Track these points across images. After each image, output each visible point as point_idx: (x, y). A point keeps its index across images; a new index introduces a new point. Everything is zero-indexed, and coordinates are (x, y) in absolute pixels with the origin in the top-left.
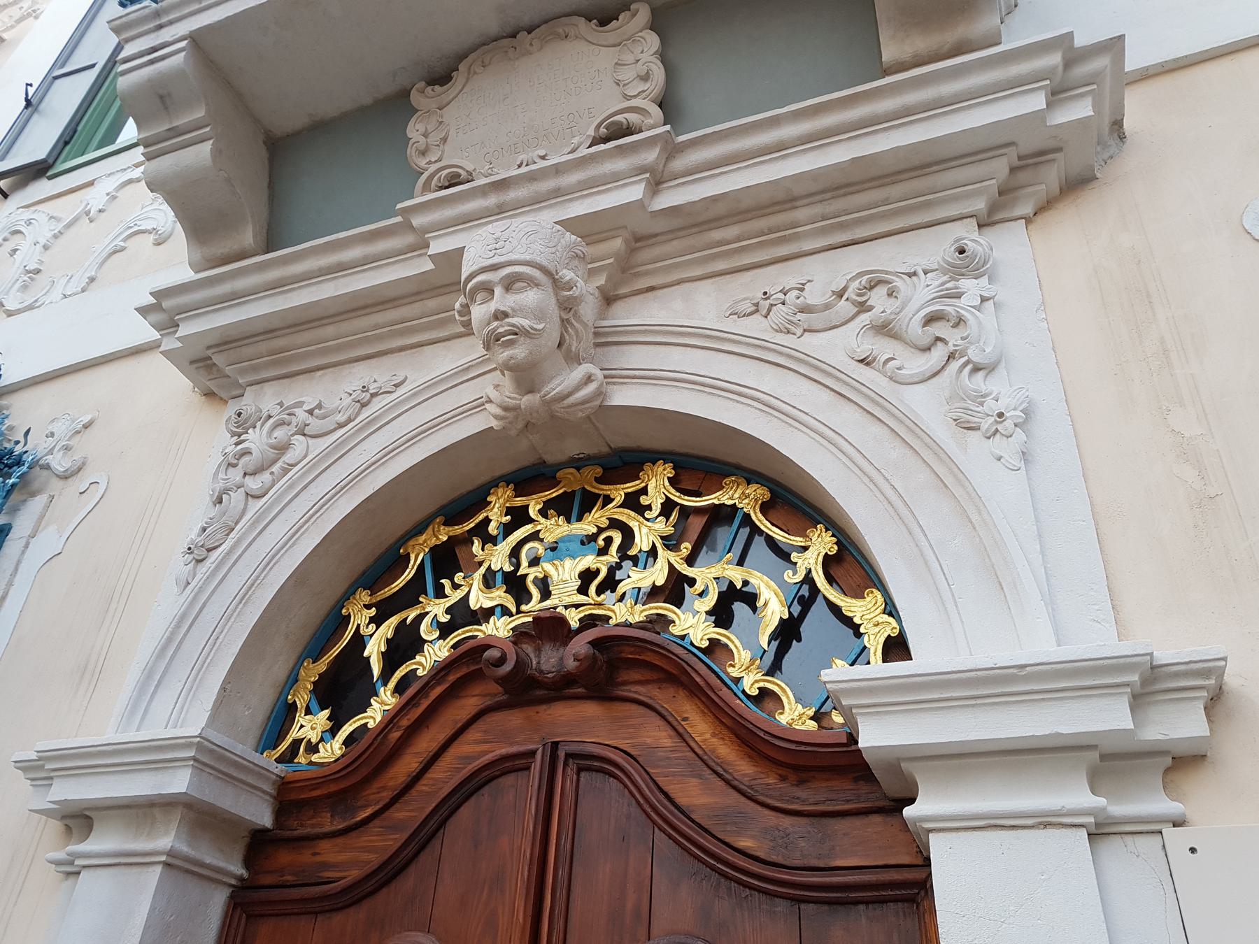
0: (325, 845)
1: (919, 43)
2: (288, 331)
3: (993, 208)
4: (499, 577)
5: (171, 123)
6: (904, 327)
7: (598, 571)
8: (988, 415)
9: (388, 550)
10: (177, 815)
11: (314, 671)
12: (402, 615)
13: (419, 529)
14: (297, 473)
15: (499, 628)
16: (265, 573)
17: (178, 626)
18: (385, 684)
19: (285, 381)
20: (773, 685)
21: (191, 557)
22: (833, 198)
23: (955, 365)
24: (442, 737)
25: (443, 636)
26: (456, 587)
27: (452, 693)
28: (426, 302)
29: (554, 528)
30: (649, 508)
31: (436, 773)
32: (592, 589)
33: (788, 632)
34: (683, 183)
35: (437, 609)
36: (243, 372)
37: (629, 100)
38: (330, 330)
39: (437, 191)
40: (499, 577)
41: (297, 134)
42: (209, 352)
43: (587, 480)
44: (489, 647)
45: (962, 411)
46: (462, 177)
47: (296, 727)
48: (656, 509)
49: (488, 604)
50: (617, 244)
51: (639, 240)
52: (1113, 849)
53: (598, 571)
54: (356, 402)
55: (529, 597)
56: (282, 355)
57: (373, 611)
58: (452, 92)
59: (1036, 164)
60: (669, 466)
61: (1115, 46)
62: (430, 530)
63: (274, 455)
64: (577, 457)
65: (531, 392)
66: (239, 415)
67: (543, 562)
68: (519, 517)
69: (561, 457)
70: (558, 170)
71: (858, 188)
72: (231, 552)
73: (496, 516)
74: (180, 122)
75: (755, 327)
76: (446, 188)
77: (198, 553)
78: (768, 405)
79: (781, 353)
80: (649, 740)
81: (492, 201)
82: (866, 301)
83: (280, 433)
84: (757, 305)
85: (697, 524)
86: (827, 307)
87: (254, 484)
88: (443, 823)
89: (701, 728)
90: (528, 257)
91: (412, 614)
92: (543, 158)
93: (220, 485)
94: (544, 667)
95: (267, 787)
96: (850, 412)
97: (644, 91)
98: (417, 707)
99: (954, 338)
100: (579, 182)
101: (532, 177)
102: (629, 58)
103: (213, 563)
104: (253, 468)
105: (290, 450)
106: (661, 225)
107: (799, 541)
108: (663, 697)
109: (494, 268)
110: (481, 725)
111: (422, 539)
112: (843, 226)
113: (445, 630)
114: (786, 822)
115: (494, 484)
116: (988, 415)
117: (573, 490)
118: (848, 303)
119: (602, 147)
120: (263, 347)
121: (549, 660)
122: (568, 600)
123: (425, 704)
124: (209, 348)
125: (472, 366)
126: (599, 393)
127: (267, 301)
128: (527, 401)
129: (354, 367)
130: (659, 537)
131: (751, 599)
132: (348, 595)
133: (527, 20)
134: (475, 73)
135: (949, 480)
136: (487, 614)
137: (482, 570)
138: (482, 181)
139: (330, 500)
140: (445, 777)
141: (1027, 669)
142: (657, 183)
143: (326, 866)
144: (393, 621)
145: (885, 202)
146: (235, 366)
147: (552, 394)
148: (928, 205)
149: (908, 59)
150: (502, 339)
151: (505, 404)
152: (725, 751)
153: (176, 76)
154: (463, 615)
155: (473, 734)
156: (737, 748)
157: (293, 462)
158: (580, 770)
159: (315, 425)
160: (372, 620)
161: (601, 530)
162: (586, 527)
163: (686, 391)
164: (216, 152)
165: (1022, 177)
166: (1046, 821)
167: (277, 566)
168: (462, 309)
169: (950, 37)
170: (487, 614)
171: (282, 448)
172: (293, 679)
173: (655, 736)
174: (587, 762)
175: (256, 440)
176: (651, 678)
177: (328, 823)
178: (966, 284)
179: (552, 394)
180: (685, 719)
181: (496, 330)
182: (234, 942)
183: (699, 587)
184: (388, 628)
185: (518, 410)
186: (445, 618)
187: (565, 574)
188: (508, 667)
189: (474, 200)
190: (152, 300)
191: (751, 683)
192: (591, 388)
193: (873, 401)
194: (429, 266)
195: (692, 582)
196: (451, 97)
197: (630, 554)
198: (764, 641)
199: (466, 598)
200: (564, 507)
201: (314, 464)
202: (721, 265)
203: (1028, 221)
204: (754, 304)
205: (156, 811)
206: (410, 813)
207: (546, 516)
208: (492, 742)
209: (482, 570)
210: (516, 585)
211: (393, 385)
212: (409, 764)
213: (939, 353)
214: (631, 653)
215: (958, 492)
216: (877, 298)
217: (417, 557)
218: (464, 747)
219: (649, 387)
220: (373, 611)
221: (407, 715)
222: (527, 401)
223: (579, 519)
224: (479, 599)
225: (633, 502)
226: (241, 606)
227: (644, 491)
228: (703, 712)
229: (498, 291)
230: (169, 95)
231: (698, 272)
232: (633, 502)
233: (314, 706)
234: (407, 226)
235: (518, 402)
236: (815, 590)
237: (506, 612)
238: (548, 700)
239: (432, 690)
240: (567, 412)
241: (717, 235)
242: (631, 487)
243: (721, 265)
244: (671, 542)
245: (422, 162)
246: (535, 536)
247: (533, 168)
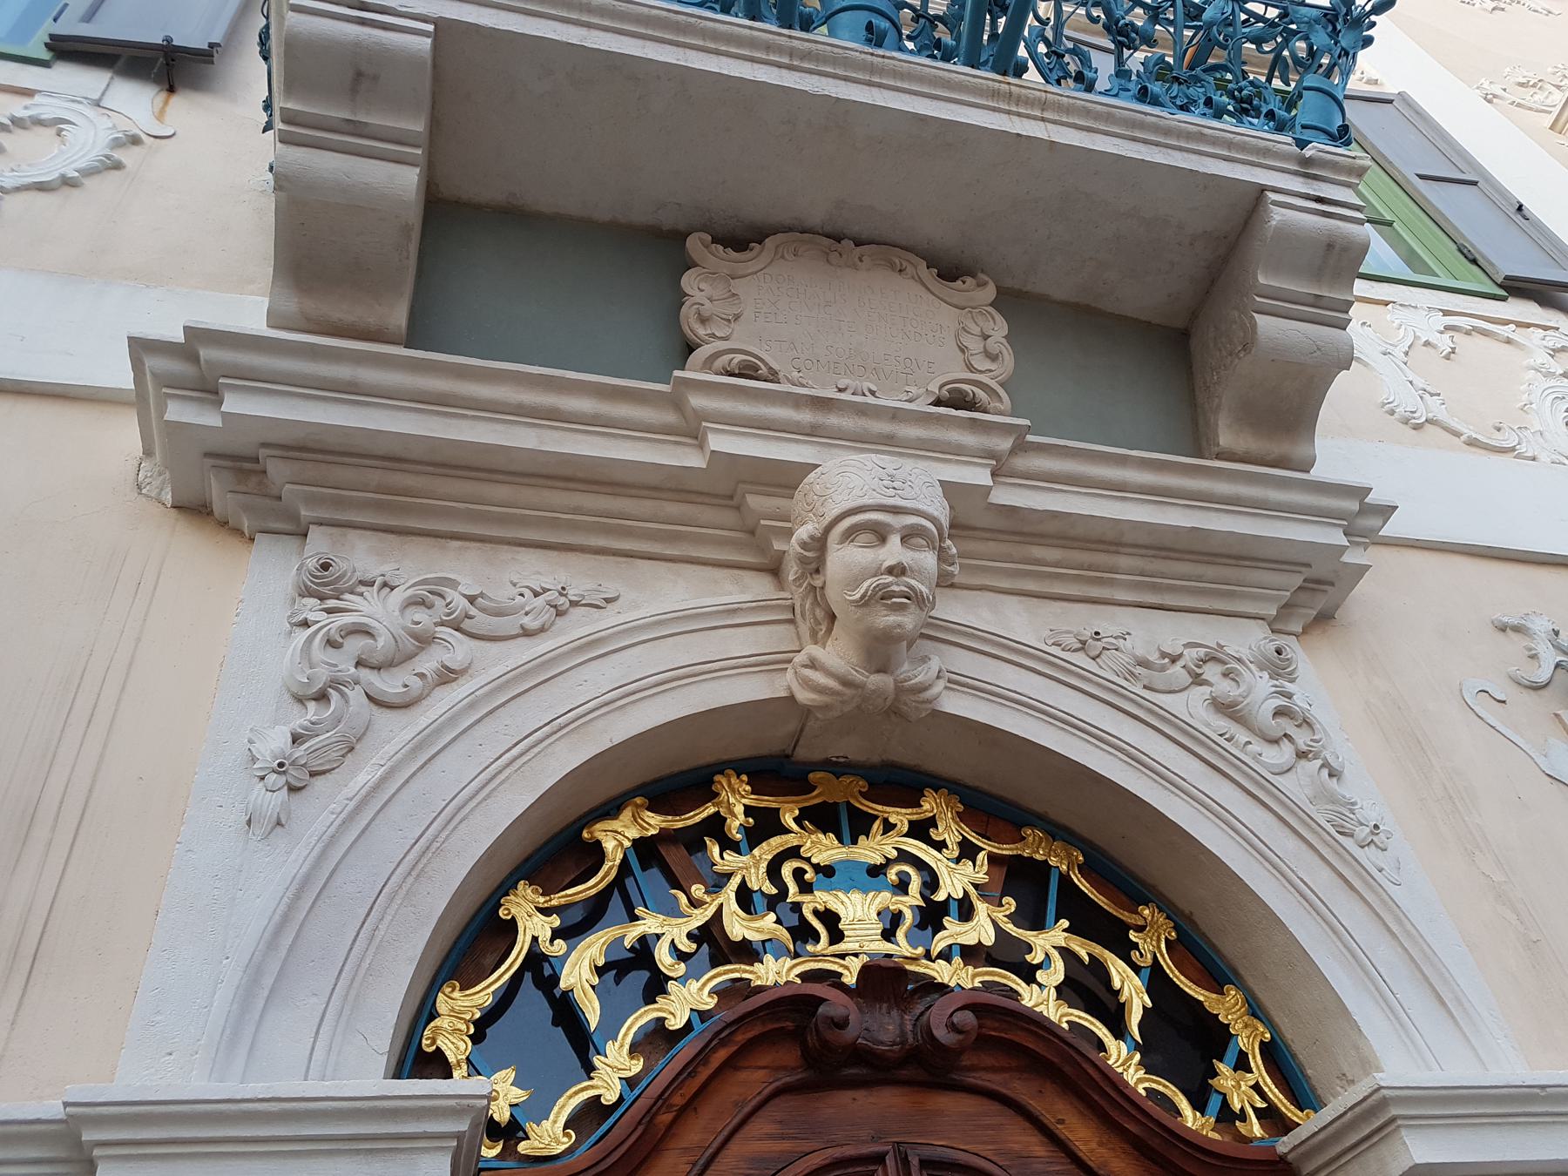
2: (430, 469)
5: (355, 115)
6: (1254, 712)
8: (1362, 824)
13: (610, 810)
14: (482, 687)
16: (446, 833)
17: (297, 897)
19: (391, 537)
21: (282, 779)
22: (1153, 556)
26: (695, 903)
28: (665, 504)
29: (824, 849)
34: (1020, 485)
36: (311, 500)
37: (972, 372)
38: (502, 492)
39: (722, 375)
42: (263, 452)
43: (850, 791)
45: (1338, 815)
46: (760, 372)
54: (552, 606)
56: (409, 499)
57: (556, 921)
58: (753, 266)
59: (1313, 589)
61: (1387, 511)
62: (627, 814)
63: (413, 648)
64: (834, 759)
65: (882, 670)
66: (325, 567)
67: (817, 890)
69: (817, 755)
70: (895, 415)
71: (1177, 555)
72: (378, 787)
74: (374, 119)
76: (732, 375)
79: (1140, 706)
80: (1016, 1147)
81: (806, 417)
82: (1201, 674)
84: (1084, 643)
92: (873, 393)
93: (323, 675)
97: (990, 371)
98: (693, 1077)
99: (1302, 738)
100: (919, 439)
101: (862, 410)
103: (351, 799)
104: (381, 658)
105: (434, 646)
109: (896, 510)
112: (1155, 588)
116: (1362, 824)
117: (835, 802)
118: (1183, 671)
120: (375, 477)
124: (265, 445)
125: (741, 609)
127: (413, 416)
128: (875, 681)
129: (518, 552)
132: (506, 887)
133: (855, 229)
134: (783, 257)
137: (734, 883)
139: (541, 741)
141: (1548, 1090)
145: (1199, 579)
146: (306, 488)
147: (913, 681)
148: (1231, 595)
149: (1240, 453)
150: (894, 600)
151: (850, 677)
156: (1135, 1162)
157: (457, 668)
159: (481, 622)
160: (556, 934)
163: (1031, 719)
167: (463, 825)
168: (811, 541)
169: (1276, 448)
171: (424, 641)
172: (425, 1012)
176: (1007, 1066)
179: (913, 681)
180: (1061, 1122)
181: (889, 586)
184: (594, 947)
185: (860, 690)
189: (781, 406)
190: (179, 337)
193: (1257, 783)
196: (750, 271)
197: (935, 899)
200: (822, 818)
201: (508, 682)
202: (1031, 586)
204: (1080, 641)
208: (796, 1138)
209: (734, 883)
211: (604, 599)
214: (995, 1029)
219: (983, 703)
220: (556, 921)
221: (681, 1089)
222: (875, 681)
226: (411, 880)
228: (1081, 1113)
229: (895, 540)
230: (375, 78)
231: (1005, 584)
234: (675, 403)
235: (865, 679)
239: (714, 1053)
240: (917, 708)
241: (1038, 552)
243: (1031, 586)
247: (869, 402)
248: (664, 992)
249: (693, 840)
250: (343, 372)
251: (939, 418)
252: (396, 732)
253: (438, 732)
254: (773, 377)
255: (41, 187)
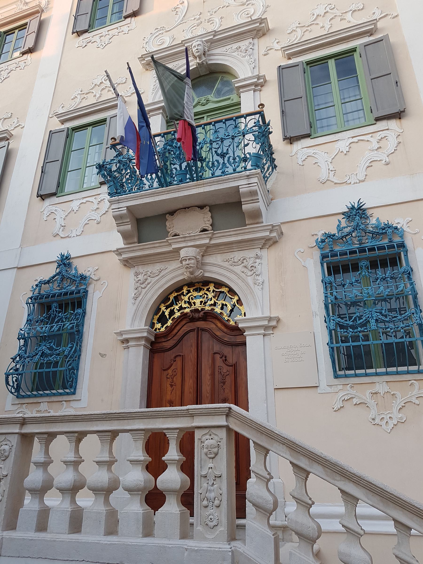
0: (163, 343)
1: (251, 222)
3: (262, 246)
4: (187, 302)
7: (203, 301)
9: (166, 297)
10: (144, 339)
11: (157, 317)
12: (171, 308)
13: (171, 293)
15: (187, 310)
18: (170, 319)
20: (229, 319)
23: (255, 274)
24: (180, 327)
25: (178, 312)
26: (179, 303)
27: (181, 321)
29: (195, 294)
30: (210, 291)
31: (180, 332)
32: (202, 304)
33: (232, 311)
35: (177, 307)
36: (134, 263)
38: (152, 257)
40: (187, 302)
41: (142, 219)
43: (200, 286)
44: (187, 314)
47: (155, 326)
48: (212, 292)
49: (185, 306)
50: (205, 248)
51: (208, 247)
52: (266, 337)
53: (203, 301)
55: (192, 305)
57: (165, 307)
60: (213, 284)
62: (173, 293)
65: (192, 275)
68: (189, 292)
73: (185, 291)
75: (226, 264)
77: (135, 298)
78: (229, 278)
81: (183, 239)
83: (145, 277)
85: (218, 293)
86: (238, 262)
87: (143, 286)
88: (182, 339)
89: (219, 325)
90: (192, 255)
91: (172, 308)
93: (136, 286)
94: (196, 316)
95: (154, 335)
96: (240, 281)
99: (255, 270)
102: (206, 216)
106: (211, 245)
107: (233, 297)
108: (214, 320)
110: (186, 325)
111: (172, 295)
113: (179, 311)
114: (231, 336)
115: (184, 285)
119: (202, 233)
120: (139, 259)
121: (197, 315)
122: (198, 306)
123: (177, 322)
126: (203, 274)
128: (191, 276)
130: (200, 233)
131: (226, 305)
132: (160, 304)
133: (187, 206)
135: (252, 292)
136: (185, 308)
137: (184, 301)
138: (181, 236)
140: (181, 333)
142: (211, 239)
143: (164, 346)
144: (169, 309)
152: (223, 328)
153: (124, 214)
154: (181, 308)
155: (185, 326)
158: (202, 331)
159: (152, 275)
160: (165, 309)
161: (203, 294)
162: (200, 294)
164: (131, 226)
165: (267, 242)
166: (259, 334)
169: (256, 221)
170: (185, 308)
171: (146, 279)
172: (153, 318)
173: (213, 326)
174: (203, 330)
175: (141, 277)
177: (163, 340)
178: (257, 260)
182: (1, 422)
183: (219, 304)
186: (178, 309)
187: (198, 301)
188: (191, 317)
191: (226, 318)
192: (202, 274)
194: (172, 249)
195: (218, 303)
198: (228, 313)
199: (181, 305)
200: (196, 290)
202: (221, 252)
203: (268, 248)
205: (140, 339)
206: (177, 338)
207: (193, 291)
209: (184, 301)
210: (189, 303)
212: (175, 331)
213: (253, 272)
215: (253, 294)
216: (245, 261)
217: (172, 298)
218: (184, 328)
220: (165, 307)
223: (199, 292)
224: (184, 306)
225: (208, 290)
227: (210, 288)
229: (187, 260)
232: (208, 290)
233: (158, 323)
236: (235, 305)
237: (188, 308)
238: (196, 321)
241: (221, 247)
242: (207, 287)
243: (221, 252)
244: (214, 297)
245: (169, 230)
246: (192, 295)
248: (175, 314)
249: (180, 295)
250: (132, 249)
251: (200, 234)
252: (144, 291)
253: (147, 291)
254: (179, 235)
255: (104, 214)
